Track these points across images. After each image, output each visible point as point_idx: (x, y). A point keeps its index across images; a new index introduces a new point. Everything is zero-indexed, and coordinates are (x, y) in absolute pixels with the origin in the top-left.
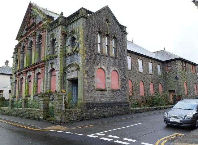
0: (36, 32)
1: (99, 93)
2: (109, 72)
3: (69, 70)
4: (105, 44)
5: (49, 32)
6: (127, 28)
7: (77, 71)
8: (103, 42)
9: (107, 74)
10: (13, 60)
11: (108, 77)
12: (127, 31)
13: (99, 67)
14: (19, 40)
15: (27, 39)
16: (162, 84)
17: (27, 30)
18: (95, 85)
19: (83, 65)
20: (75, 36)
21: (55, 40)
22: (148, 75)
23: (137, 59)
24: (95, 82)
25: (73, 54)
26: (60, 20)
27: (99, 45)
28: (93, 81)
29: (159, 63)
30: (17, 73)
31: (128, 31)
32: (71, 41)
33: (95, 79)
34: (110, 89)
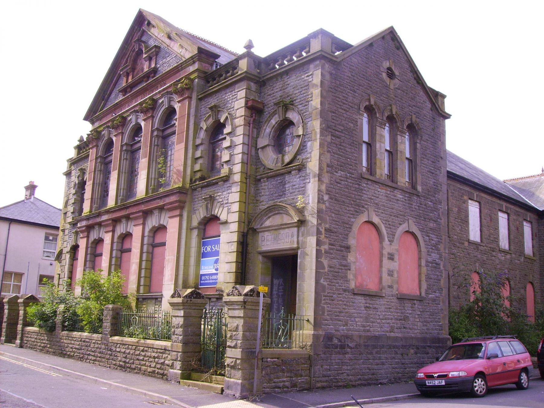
0: (155, 98)
1: (360, 300)
2: (392, 235)
3: (268, 223)
4: (382, 145)
5: (200, 99)
6: (445, 100)
7: (296, 229)
8: (378, 138)
9: (386, 242)
10: (68, 183)
11: (389, 254)
12: (448, 109)
13: (364, 218)
14: (93, 123)
15: (125, 119)
16: (535, 285)
17: (124, 91)
18: (350, 276)
19: (319, 211)
20: (293, 116)
21: (222, 126)
22: (494, 253)
23: (465, 198)
24: (353, 267)
25: (282, 174)
26: (243, 65)
27: (364, 147)
28: (344, 262)
29: (529, 215)
30: (84, 223)
31: (449, 107)
32: (275, 132)
33: (351, 258)
34: (395, 292)
